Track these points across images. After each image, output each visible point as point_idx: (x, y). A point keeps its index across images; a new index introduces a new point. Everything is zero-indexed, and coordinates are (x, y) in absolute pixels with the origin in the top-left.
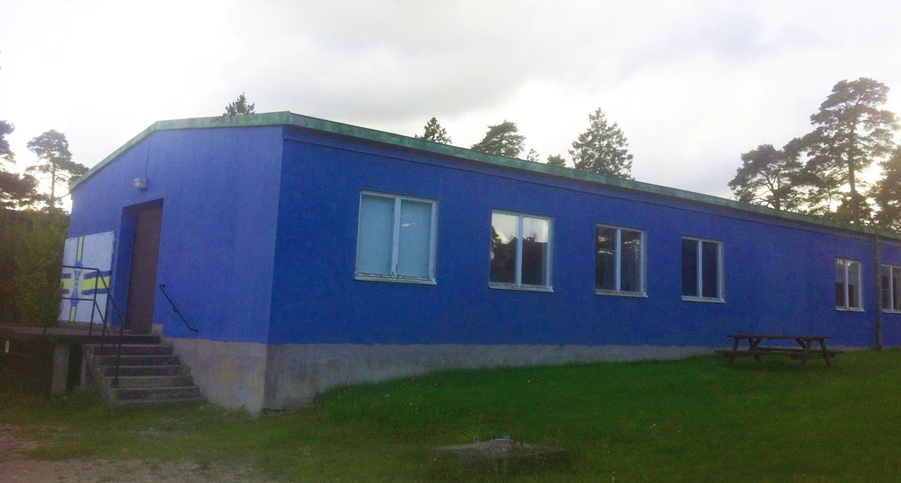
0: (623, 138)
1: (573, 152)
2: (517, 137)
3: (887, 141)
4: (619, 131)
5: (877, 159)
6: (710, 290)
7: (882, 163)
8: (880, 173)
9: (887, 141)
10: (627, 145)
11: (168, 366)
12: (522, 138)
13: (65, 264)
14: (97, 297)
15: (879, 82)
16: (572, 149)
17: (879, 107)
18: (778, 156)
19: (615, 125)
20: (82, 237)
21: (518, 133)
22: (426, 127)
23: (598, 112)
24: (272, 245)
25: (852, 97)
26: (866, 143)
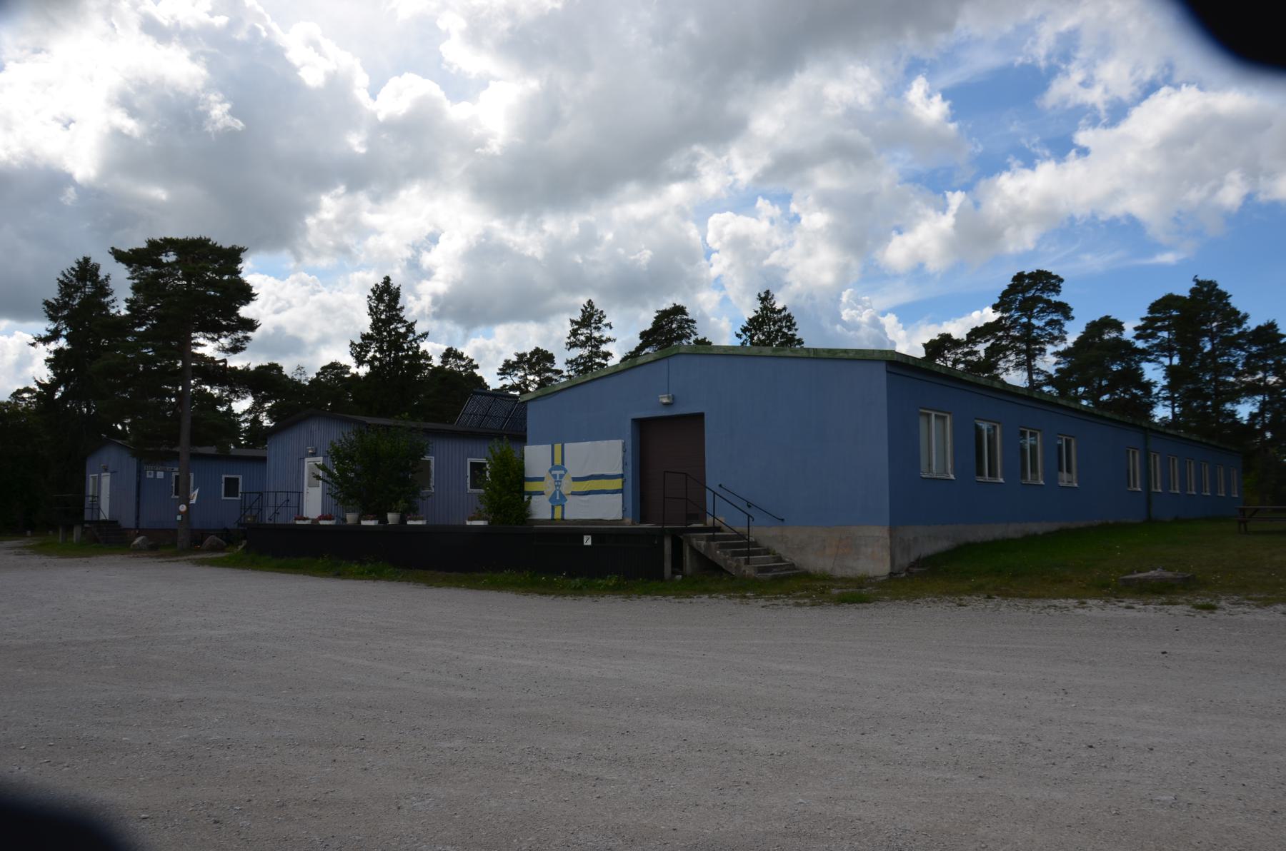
0: (793, 322)
1: (741, 335)
2: (687, 321)
3: (1060, 330)
4: (789, 316)
5: (1050, 348)
6: (992, 473)
7: (1056, 354)
8: (429, 334)
9: (1060, 330)
10: (796, 330)
11: (807, 584)
12: (693, 322)
13: (528, 474)
14: (550, 514)
15: (1054, 274)
16: (740, 332)
17: (1054, 298)
18: (958, 344)
19: (785, 309)
20: (560, 445)
21: (690, 317)
22: (582, 310)
23: (767, 292)
24: (544, 446)
25: (1029, 287)
26: (1039, 332)
